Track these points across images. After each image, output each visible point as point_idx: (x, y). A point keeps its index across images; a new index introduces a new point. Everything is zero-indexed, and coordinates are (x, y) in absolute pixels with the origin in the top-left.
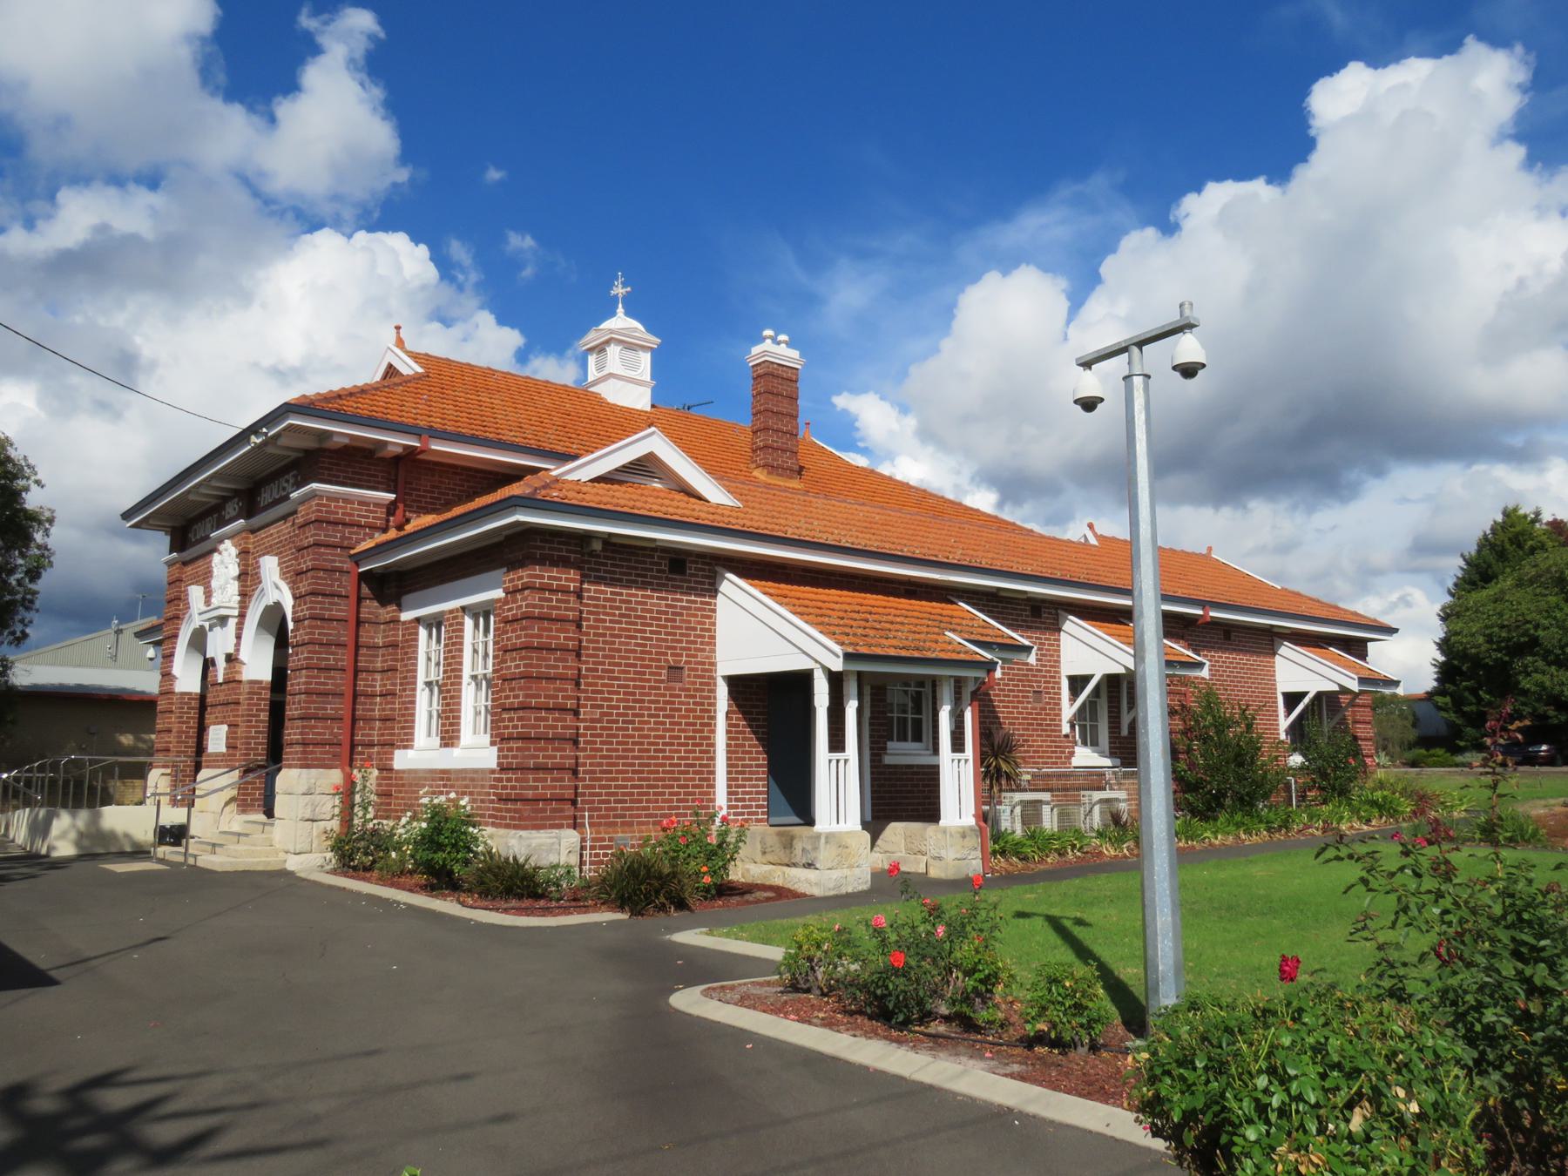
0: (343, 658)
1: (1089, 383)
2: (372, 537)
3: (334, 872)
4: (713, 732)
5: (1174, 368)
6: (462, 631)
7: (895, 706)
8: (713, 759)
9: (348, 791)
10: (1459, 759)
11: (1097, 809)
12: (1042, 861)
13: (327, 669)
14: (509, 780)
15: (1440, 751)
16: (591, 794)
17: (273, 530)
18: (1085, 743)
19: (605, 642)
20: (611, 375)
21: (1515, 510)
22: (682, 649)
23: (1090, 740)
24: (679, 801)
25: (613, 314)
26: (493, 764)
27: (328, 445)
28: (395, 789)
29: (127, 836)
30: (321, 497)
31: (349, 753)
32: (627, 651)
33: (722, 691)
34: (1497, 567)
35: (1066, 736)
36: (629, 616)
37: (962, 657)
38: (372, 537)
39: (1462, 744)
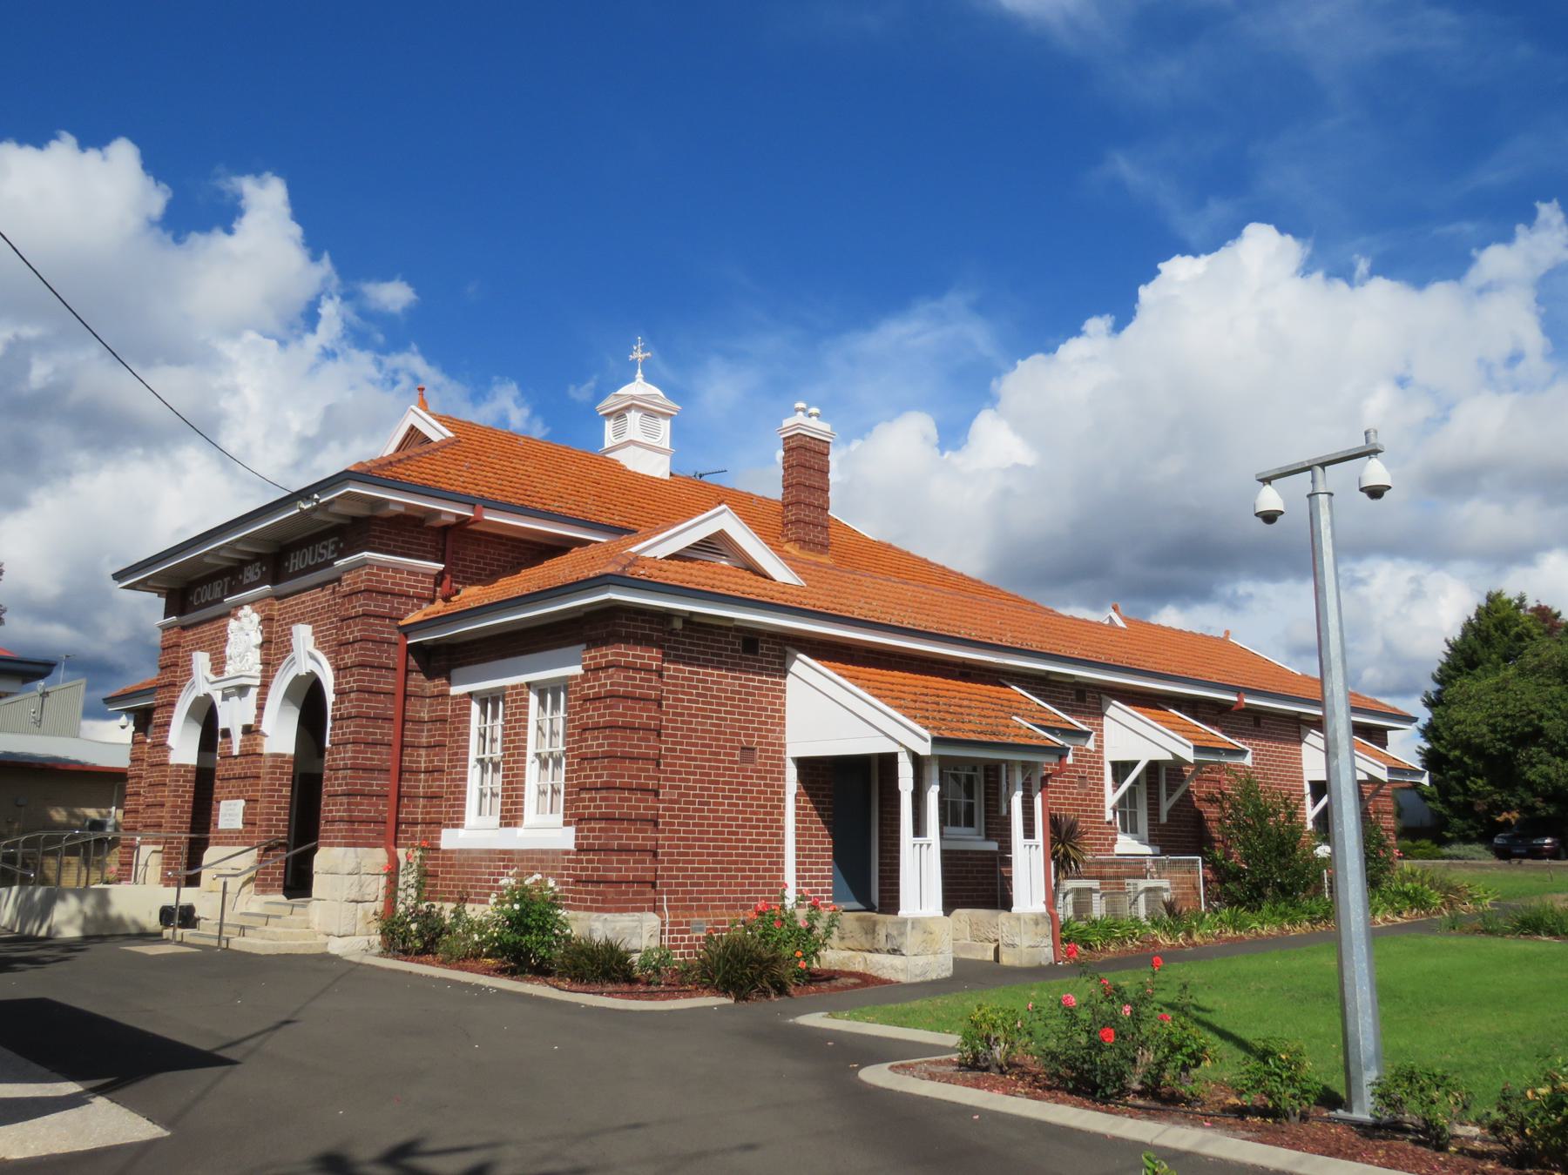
0: (388, 732)
1: (1270, 498)
2: (420, 608)
3: (381, 955)
4: (782, 814)
5: (1362, 490)
6: (527, 707)
7: (975, 787)
8: (782, 842)
9: (393, 873)
10: (1446, 851)
11: (1142, 898)
12: (1104, 950)
13: (375, 744)
14: (589, 861)
15: (1426, 843)
16: (670, 877)
17: (305, 597)
18: (1124, 830)
19: (683, 722)
20: (631, 442)
21: (1499, 595)
22: (755, 729)
23: (1130, 827)
24: (751, 884)
25: (633, 380)
26: (571, 846)
27: (383, 513)
28: (439, 872)
29: (135, 922)
30: (372, 566)
31: (391, 832)
32: (703, 731)
33: (791, 773)
34: (1482, 653)
35: (1109, 823)
36: (705, 696)
37: (1035, 742)
38: (420, 608)
39: (1449, 835)
